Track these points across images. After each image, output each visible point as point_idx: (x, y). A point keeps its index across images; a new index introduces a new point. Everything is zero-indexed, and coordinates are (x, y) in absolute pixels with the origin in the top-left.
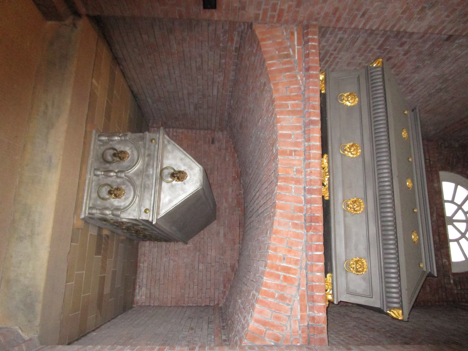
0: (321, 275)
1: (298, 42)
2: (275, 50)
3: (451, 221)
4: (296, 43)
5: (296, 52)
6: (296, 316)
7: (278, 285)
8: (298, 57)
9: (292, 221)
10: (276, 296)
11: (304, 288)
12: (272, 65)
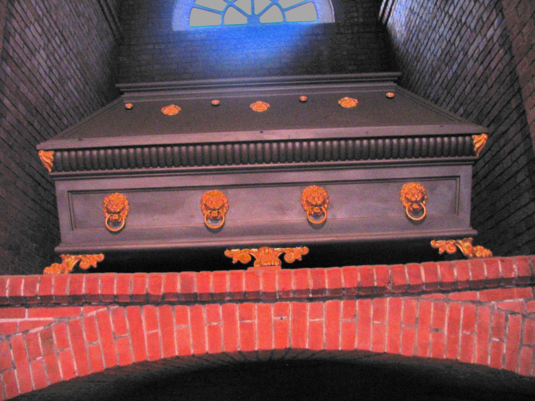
0: (456, 268)
1: (17, 317)
2: (34, 362)
3: (253, 17)
4: (19, 320)
5: (36, 319)
6: (521, 304)
7: (480, 338)
8: (49, 316)
9: (372, 319)
10: (497, 340)
11: (478, 293)
12: (68, 366)
